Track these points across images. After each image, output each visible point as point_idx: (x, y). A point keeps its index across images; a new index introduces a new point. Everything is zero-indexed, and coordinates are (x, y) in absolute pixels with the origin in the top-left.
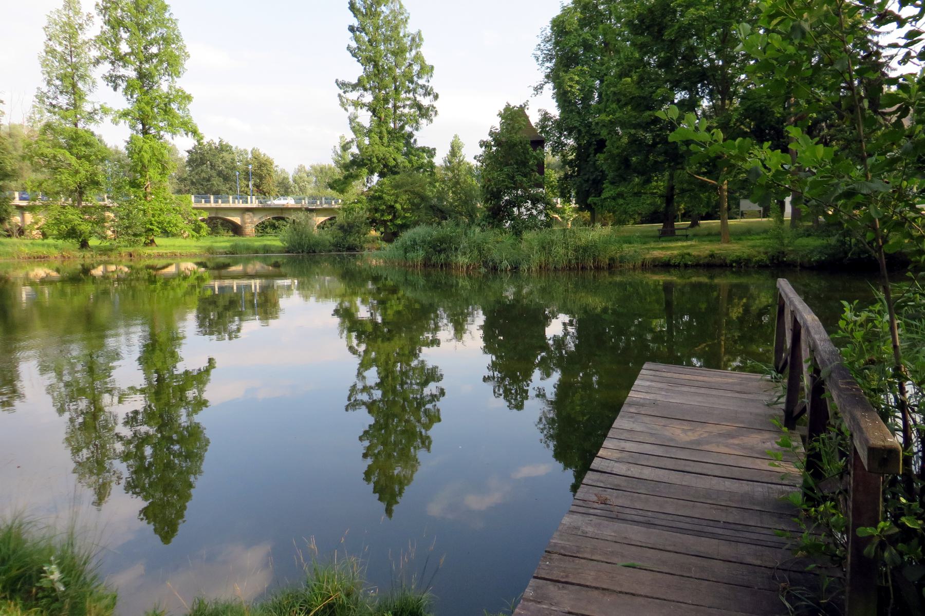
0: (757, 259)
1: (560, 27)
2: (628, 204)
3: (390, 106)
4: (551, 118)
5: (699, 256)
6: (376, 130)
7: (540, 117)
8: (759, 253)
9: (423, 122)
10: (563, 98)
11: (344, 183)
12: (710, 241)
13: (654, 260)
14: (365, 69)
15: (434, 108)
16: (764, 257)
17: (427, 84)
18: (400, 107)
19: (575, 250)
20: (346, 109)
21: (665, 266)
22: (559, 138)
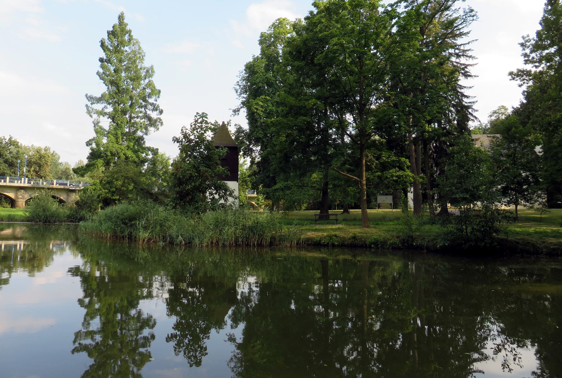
0: (391, 241)
1: (251, 69)
2: (293, 194)
3: (127, 116)
4: (244, 131)
5: (344, 237)
6: (113, 132)
7: (236, 130)
8: (393, 236)
9: (152, 129)
10: (252, 117)
11: (85, 170)
12: (354, 225)
13: (308, 240)
14: (108, 88)
15: (161, 120)
16: (397, 241)
17: (155, 102)
18: (134, 117)
19: (243, 229)
20: (91, 116)
21: (316, 245)
22: (249, 145)
